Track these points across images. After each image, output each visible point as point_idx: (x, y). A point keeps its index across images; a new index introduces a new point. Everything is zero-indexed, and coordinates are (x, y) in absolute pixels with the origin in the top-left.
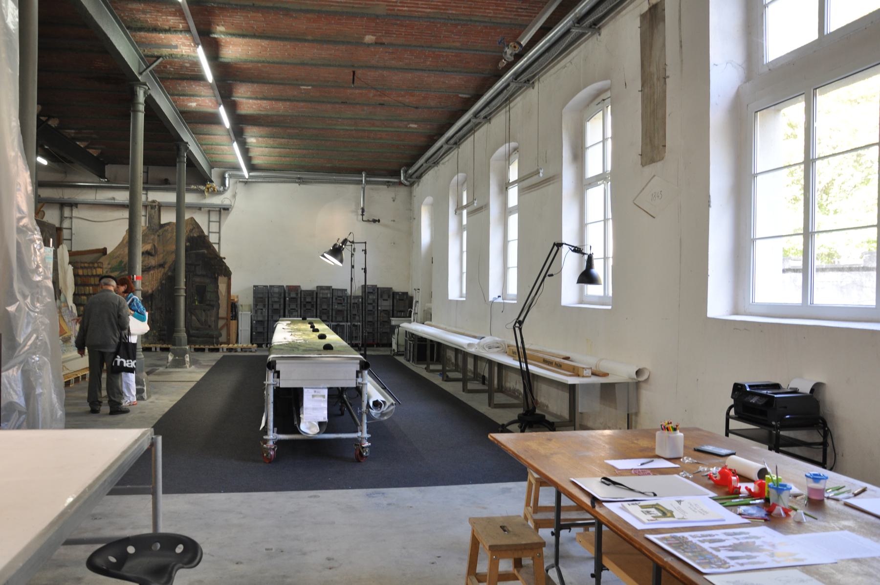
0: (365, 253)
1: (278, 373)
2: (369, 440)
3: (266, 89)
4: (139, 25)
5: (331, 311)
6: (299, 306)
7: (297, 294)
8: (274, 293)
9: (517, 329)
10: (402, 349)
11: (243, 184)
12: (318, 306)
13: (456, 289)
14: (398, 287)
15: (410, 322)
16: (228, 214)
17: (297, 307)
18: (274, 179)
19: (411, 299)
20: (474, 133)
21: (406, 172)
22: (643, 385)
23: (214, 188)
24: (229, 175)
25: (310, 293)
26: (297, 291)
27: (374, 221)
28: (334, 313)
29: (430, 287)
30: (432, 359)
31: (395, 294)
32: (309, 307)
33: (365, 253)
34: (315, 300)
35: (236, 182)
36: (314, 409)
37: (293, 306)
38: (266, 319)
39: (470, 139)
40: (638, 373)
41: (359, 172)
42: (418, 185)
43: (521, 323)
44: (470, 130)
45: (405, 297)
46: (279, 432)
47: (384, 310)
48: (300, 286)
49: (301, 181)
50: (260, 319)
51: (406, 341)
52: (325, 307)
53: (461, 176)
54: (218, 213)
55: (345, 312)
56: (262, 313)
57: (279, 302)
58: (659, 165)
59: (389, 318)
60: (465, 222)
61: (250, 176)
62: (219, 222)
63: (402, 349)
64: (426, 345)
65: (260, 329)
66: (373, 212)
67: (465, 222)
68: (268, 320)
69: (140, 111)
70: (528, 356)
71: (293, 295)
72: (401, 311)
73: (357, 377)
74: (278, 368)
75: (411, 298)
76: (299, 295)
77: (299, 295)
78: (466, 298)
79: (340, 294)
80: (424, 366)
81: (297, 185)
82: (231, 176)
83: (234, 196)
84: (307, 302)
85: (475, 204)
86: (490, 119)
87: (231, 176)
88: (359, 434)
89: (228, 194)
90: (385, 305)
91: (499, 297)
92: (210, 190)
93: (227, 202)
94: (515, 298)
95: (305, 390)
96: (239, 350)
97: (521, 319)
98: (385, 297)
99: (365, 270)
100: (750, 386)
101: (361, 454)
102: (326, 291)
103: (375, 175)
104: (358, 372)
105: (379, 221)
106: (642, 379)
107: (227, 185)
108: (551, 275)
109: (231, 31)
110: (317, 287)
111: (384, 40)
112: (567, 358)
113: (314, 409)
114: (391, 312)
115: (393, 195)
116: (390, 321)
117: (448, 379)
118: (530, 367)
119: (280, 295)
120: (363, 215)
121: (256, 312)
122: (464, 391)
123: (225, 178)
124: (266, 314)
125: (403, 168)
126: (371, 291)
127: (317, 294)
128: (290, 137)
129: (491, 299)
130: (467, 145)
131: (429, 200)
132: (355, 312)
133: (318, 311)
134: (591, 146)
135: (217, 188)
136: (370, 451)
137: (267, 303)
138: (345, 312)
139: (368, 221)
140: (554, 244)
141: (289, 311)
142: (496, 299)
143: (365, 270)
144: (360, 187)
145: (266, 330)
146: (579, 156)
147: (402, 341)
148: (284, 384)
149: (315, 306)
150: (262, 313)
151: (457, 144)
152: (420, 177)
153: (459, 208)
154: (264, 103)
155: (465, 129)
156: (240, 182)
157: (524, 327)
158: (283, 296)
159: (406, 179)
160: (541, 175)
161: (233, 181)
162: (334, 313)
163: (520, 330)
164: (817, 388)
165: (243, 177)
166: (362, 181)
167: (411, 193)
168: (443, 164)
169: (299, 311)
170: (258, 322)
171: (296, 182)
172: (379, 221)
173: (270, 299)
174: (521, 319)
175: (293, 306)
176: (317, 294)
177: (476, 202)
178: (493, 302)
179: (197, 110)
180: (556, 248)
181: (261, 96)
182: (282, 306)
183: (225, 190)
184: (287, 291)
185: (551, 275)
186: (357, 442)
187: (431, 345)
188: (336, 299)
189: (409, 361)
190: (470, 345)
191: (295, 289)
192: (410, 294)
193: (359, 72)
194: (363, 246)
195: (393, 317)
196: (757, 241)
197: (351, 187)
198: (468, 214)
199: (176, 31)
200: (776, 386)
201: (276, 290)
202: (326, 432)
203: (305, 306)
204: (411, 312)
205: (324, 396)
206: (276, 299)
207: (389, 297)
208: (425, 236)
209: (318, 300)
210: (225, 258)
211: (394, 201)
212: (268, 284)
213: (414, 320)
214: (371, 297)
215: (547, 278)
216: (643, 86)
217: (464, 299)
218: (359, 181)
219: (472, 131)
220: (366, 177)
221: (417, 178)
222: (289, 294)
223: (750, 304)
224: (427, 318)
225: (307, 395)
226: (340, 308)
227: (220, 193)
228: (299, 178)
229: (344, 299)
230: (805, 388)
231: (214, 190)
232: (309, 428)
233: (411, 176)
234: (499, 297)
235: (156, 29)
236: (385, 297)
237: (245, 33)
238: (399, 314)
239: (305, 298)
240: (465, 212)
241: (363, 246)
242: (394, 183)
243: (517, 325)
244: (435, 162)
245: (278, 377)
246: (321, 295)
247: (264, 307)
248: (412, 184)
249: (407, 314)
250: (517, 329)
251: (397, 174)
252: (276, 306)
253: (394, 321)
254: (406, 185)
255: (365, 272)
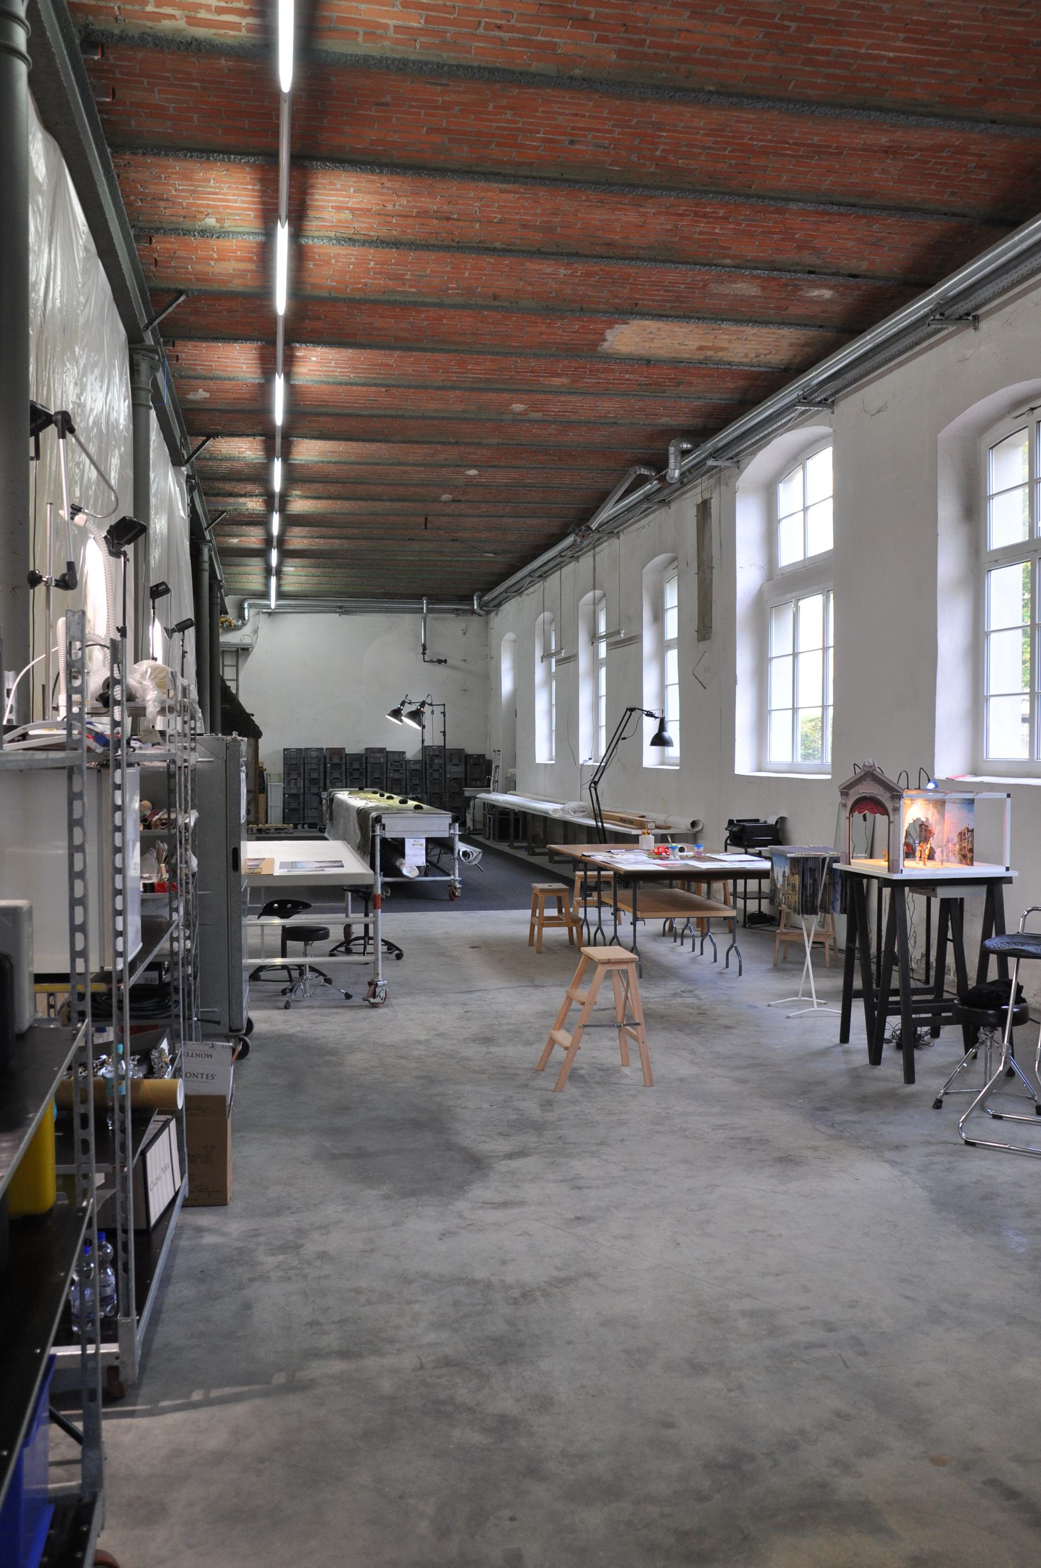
0: (444, 716)
1: (384, 827)
2: (460, 882)
3: (324, 531)
4: (216, 491)
5: (385, 780)
6: (344, 774)
7: (341, 759)
8: (311, 758)
9: (592, 789)
10: (480, 826)
11: (267, 615)
12: (369, 774)
13: (543, 752)
14: (472, 748)
15: (489, 792)
16: (248, 655)
17: (341, 775)
18: (307, 609)
19: (489, 763)
20: (562, 568)
21: (480, 598)
22: (699, 835)
23: (230, 623)
24: (249, 604)
25: (357, 757)
26: (341, 754)
27: (440, 662)
28: (389, 782)
29: (514, 745)
30: (516, 838)
31: (468, 757)
32: (356, 775)
33: (444, 716)
34: (364, 766)
35: (258, 613)
36: (414, 856)
37: (336, 775)
38: (302, 792)
39: (557, 574)
40: (694, 824)
41: (419, 597)
42: (497, 614)
43: (596, 783)
44: (558, 564)
45: (481, 761)
46: (385, 876)
47: (454, 779)
48: (344, 749)
49: (344, 611)
50: (294, 791)
51: (484, 815)
52: (377, 775)
53: (547, 615)
54: (235, 654)
55: (404, 781)
56: (296, 785)
57: (319, 769)
58: (708, 642)
59: (461, 788)
60: (553, 669)
61: (277, 606)
62: (237, 666)
63: (480, 826)
64: (508, 820)
65: (294, 806)
66: (439, 649)
67: (553, 669)
68: (304, 793)
69: (205, 570)
70: (603, 816)
71: (336, 760)
72: (477, 780)
73: (450, 829)
74: (383, 821)
75: (490, 762)
76: (344, 760)
77: (344, 760)
78: (832, 774)
79: (396, 758)
80: (507, 844)
81: (337, 615)
82: (250, 606)
83: (256, 631)
84: (354, 770)
85: (563, 655)
86: (578, 557)
87: (250, 606)
88: (452, 877)
89: (247, 630)
90: (455, 771)
91: (590, 759)
92: (225, 625)
93: (247, 641)
94: (678, 761)
95: (406, 840)
96: (273, 831)
97: (596, 779)
98: (455, 761)
99: (444, 733)
100: (737, 821)
101: (454, 894)
102: (379, 755)
103: (441, 601)
104: (450, 825)
105: (445, 661)
106: (696, 829)
107: (246, 618)
108: (624, 738)
109: (307, 494)
110: (366, 749)
111: (461, 498)
112: (643, 817)
113: (414, 856)
114: (464, 780)
115: (463, 626)
116: (463, 791)
117: (534, 854)
118: (605, 825)
119: (320, 761)
120: (424, 654)
121: (289, 782)
122: (550, 862)
123: (244, 608)
124: (302, 786)
125: (476, 594)
126: (437, 753)
127: (366, 758)
128: (339, 566)
129: (581, 762)
130: (554, 579)
131: (510, 636)
132: (416, 782)
133: (369, 781)
134: (338, 923)
135: (234, 622)
136: (462, 892)
137: (302, 771)
138: (404, 781)
139: (431, 661)
140: (627, 709)
141: (331, 781)
142: (585, 760)
143: (444, 733)
144: (420, 616)
145: (301, 806)
146: (658, 617)
147: (479, 817)
148: (389, 835)
149: (364, 774)
150: (296, 785)
151: (543, 577)
152: (499, 605)
153: (547, 656)
154: (322, 541)
155: (551, 564)
156: (263, 613)
157: (599, 787)
158: (322, 761)
159: (480, 607)
160: (622, 635)
161: (253, 611)
162: (389, 782)
163: (596, 789)
164: (782, 820)
165: (268, 607)
166: (423, 609)
167: (487, 623)
168: (527, 595)
169: (344, 780)
170: (291, 795)
171: (336, 612)
172: (445, 661)
173: (306, 766)
174: (596, 779)
175: (336, 775)
176: (366, 758)
177: (563, 651)
178: (583, 765)
179: (238, 546)
180: (628, 713)
181: (318, 535)
182: (322, 776)
183: (244, 624)
184: (328, 756)
185: (624, 738)
186: (450, 885)
187: (515, 819)
188: (392, 764)
189: (488, 839)
190: (555, 810)
191: (339, 752)
192: (487, 757)
193: (430, 518)
194: (441, 709)
195: (466, 787)
196: (773, 712)
197: (408, 617)
198: (557, 661)
199: (251, 496)
200: (757, 821)
201: (314, 754)
202: (426, 875)
203: (351, 774)
204: (489, 780)
205: (422, 845)
206: (314, 766)
207: (460, 761)
208: (507, 684)
209: (369, 766)
210: (253, 715)
211: (465, 634)
212: (303, 747)
213: (494, 790)
214: (436, 761)
215: (620, 741)
216: (698, 570)
217: (553, 762)
218: (418, 608)
219: (560, 566)
220: (428, 604)
221: (494, 606)
222: (331, 759)
223: (984, 761)
224: (511, 786)
225: (409, 844)
226: (397, 776)
227: (237, 628)
228: (340, 607)
229: (402, 764)
230: (772, 820)
231: (230, 625)
232: (410, 872)
233: (486, 604)
234: (590, 759)
235: (231, 495)
236: (455, 761)
237: (320, 495)
238: (473, 783)
239: (351, 764)
240: (553, 661)
241: (441, 709)
242: (465, 611)
243: (593, 785)
244: (518, 591)
245: (384, 829)
246: (372, 760)
247: (299, 776)
248: (488, 613)
249: (485, 785)
250: (592, 789)
251: (469, 599)
252: (314, 775)
253: (468, 792)
254: (480, 616)
255: (444, 735)
